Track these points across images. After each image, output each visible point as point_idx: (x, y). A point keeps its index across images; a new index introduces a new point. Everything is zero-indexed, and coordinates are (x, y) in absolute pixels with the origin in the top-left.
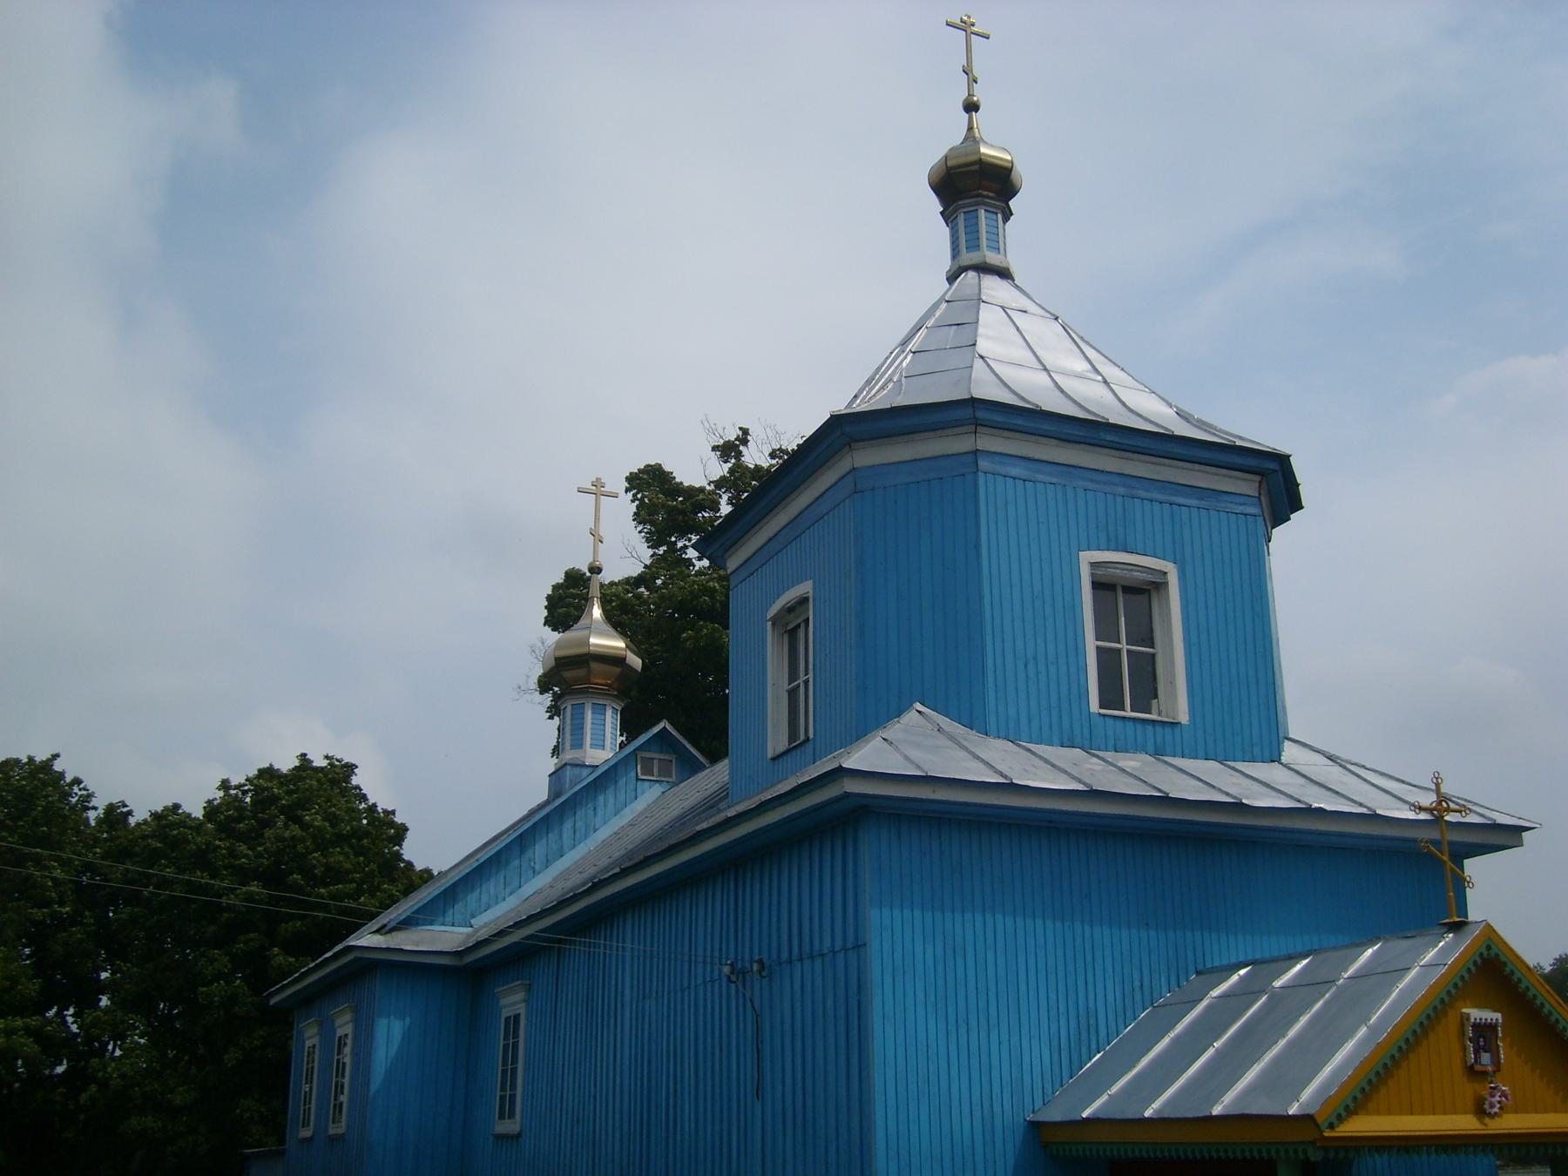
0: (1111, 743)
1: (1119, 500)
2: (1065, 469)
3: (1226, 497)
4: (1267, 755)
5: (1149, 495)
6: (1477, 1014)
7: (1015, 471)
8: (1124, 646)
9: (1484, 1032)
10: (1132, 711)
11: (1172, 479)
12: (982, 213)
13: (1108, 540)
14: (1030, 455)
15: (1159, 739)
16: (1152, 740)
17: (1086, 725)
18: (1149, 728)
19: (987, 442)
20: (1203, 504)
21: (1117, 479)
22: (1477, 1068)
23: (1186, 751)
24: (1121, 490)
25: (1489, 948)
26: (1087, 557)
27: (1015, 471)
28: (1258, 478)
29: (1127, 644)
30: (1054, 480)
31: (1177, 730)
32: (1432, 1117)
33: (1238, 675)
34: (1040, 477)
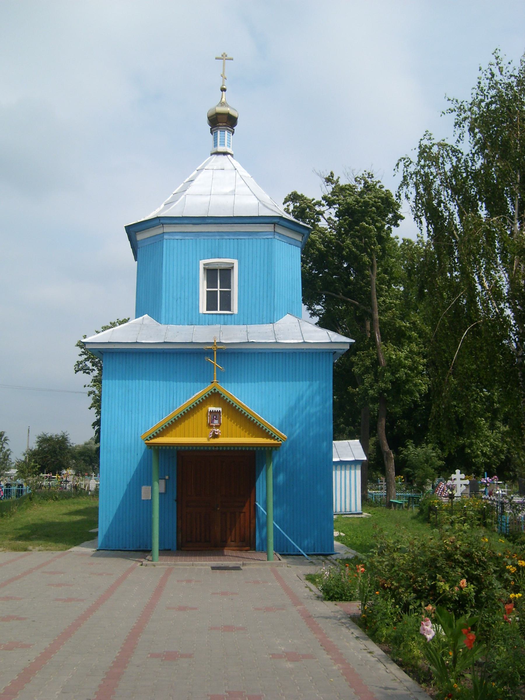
0: (207, 322)
1: (217, 241)
2: (197, 233)
3: (261, 234)
4: (268, 322)
5: (228, 237)
6: (211, 408)
7: (177, 237)
8: (219, 289)
9: (215, 415)
10: (220, 310)
11: (238, 231)
12: (219, 132)
13: (212, 255)
14: (183, 231)
15: (225, 319)
16: (223, 320)
17: (198, 318)
18: (218, 316)
19: (167, 229)
20: (250, 237)
21: (216, 234)
22: (211, 424)
23: (236, 323)
24: (218, 237)
25: (215, 390)
26: (202, 262)
27: (177, 237)
28: (273, 225)
29: (220, 288)
30: (192, 238)
31: (233, 316)
32: (243, 438)
33: (260, 296)
34: (187, 238)
